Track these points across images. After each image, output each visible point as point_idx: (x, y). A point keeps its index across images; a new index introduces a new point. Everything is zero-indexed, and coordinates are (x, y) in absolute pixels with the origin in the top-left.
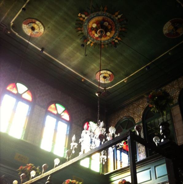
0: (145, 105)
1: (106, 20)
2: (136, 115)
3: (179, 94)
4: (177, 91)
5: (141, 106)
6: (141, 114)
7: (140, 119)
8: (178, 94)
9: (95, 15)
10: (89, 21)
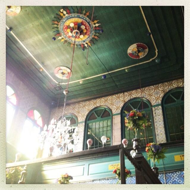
0: (90, 108)
1: (85, 24)
2: (80, 114)
3: (122, 106)
4: (121, 103)
5: (87, 107)
6: (85, 115)
7: (84, 118)
8: (162, 96)
9: (75, 16)
10: (68, 19)
